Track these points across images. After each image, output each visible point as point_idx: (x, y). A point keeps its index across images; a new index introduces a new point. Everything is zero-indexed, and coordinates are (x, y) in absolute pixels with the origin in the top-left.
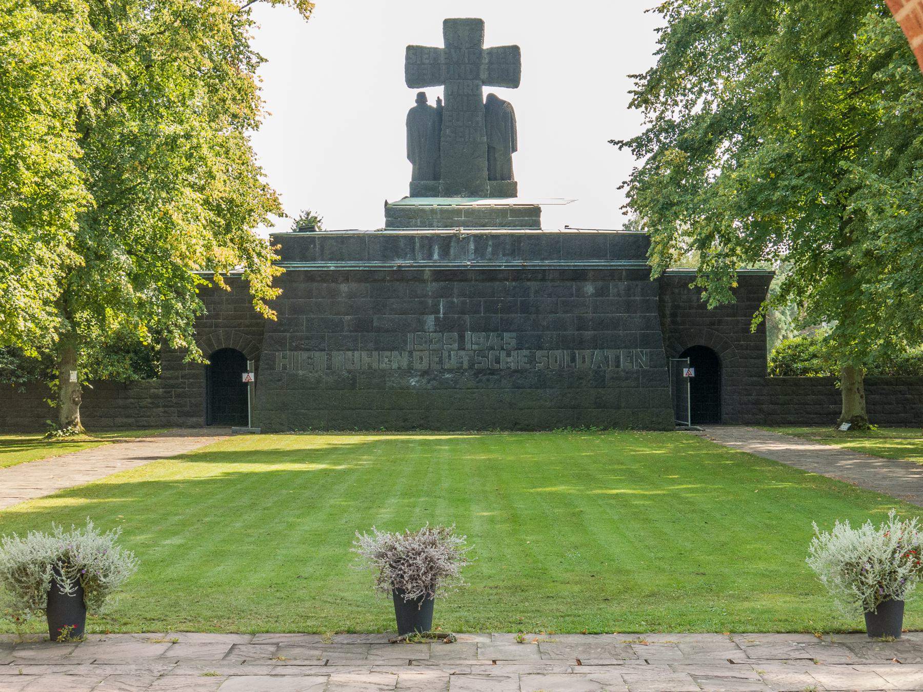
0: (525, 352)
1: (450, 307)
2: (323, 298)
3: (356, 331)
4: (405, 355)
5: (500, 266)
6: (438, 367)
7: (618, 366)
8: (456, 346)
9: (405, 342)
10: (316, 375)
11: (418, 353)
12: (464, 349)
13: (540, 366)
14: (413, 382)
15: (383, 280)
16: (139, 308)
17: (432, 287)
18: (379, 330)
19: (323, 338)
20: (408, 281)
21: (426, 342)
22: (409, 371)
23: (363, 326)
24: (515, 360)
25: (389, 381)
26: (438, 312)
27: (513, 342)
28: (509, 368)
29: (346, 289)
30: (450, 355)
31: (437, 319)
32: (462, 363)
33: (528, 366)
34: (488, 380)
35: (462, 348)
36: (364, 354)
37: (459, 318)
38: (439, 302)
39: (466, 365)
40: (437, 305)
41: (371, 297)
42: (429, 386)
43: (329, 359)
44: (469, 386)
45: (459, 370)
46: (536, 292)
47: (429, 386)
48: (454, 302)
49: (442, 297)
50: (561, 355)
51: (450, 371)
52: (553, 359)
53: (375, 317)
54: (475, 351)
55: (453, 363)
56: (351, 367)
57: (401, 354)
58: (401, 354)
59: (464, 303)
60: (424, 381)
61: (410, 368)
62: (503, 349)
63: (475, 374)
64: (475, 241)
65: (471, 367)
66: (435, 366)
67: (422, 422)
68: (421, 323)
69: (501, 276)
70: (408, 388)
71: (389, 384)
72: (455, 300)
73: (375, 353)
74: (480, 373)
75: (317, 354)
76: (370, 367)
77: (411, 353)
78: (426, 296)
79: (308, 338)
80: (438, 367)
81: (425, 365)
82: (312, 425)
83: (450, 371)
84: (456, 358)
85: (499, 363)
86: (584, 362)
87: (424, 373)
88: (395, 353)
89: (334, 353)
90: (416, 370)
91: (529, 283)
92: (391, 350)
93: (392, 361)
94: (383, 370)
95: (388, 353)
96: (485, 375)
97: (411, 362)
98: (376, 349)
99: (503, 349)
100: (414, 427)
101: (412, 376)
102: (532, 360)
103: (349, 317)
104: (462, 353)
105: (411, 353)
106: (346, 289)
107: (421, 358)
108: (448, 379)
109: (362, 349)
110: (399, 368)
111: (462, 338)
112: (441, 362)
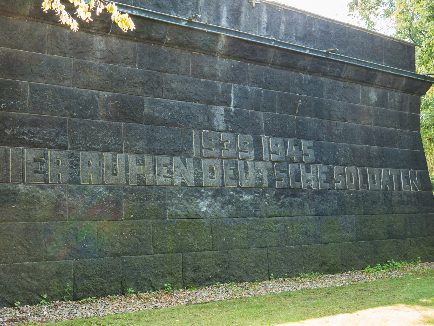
0: (324, 168)
1: (244, 96)
2: (64, 54)
3: (117, 119)
4: (190, 162)
5: (304, 49)
6: (232, 183)
7: (400, 188)
8: (251, 154)
9: (190, 143)
10: (51, 192)
11: (208, 161)
12: (261, 159)
13: (338, 185)
14: (203, 206)
15: (160, 41)
16: (61, 276)
17: (222, 65)
18: (151, 121)
19: (62, 125)
20: (194, 48)
21: (216, 146)
22: (197, 189)
23: (128, 112)
24: (313, 178)
25: (172, 205)
26: (227, 103)
27: (312, 154)
28: (310, 188)
29: (102, 46)
30: (246, 167)
31: (227, 111)
32: (261, 179)
33: (327, 185)
34: (291, 204)
35: (259, 158)
36: (131, 158)
37: (252, 114)
38: (230, 87)
39: (266, 183)
40: (227, 92)
41: (140, 66)
42: (224, 214)
43: (75, 165)
44: (271, 213)
45: (257, 189)
46: (330, 91)
47: (224, 214)
48: (246, 92)
49: (233, 81)
50: (354, 172)
51: (248, 190)
52: (349, 177)
53: (146, 99)
54: (273, 162)
55: (248, 179)
56: (110, 180)
57: (184, 162)
58: (184, 162)
59: (258, 94)
60: (217, 205)
61: (199, 185)
62: (302, 162)
63: (276, 195)
64: (268, 12)
65: (271, 186)
66: (230, 183)
67: (218, 270)
68: (210, 116)
69: (301, 63)
70: (197, 216)
71: (171, 210)
72: (248, 88)
73: (148, 158)
74: (281, 194)
75: (52, 154)
76: (142, 182)
77: (198, 160)
78: (214, 76)
79: (35, 123)
80: (232, 183)
81: (214, 181)
82: (47, 290)
83: (248, 190)
84: (254, 173)
85: (299, 180)
86: (374, 183)
87: (218, 193)
88: (176, 160)
89: (82, 155)
90: (206, 188)
91: (322, 79)
92: (171, 155)
93: (175, 172)
94: (161, 187)
95: (166, 160)
96: (286, 197)
97: (198, 175)
98: (150, 152)
99: (302, 162)
100: (209, 279)
101: (202, 197)
102: (330, 178)
103: (106, 94)
104: (260, 164)
105: (198, 160)
106: (102, 46)
107: (211, 170)
108: (245, 202)
109: (128, 150)
110: (184, 184)
111: (258, 142)
112: (236, 177)
